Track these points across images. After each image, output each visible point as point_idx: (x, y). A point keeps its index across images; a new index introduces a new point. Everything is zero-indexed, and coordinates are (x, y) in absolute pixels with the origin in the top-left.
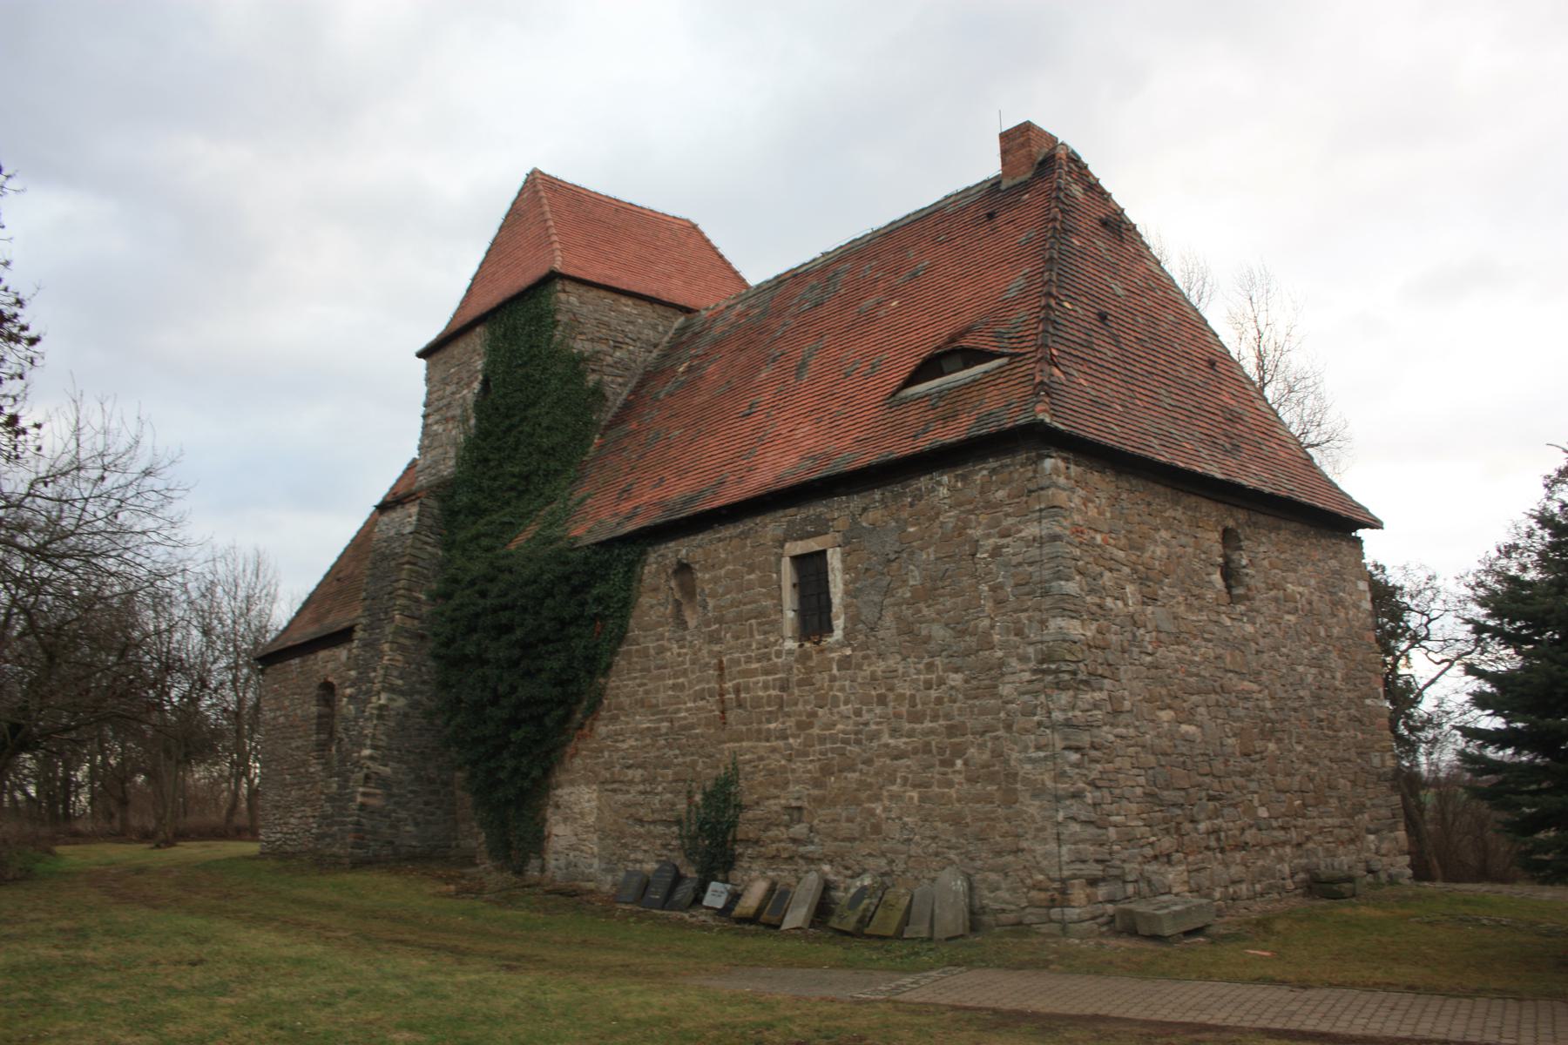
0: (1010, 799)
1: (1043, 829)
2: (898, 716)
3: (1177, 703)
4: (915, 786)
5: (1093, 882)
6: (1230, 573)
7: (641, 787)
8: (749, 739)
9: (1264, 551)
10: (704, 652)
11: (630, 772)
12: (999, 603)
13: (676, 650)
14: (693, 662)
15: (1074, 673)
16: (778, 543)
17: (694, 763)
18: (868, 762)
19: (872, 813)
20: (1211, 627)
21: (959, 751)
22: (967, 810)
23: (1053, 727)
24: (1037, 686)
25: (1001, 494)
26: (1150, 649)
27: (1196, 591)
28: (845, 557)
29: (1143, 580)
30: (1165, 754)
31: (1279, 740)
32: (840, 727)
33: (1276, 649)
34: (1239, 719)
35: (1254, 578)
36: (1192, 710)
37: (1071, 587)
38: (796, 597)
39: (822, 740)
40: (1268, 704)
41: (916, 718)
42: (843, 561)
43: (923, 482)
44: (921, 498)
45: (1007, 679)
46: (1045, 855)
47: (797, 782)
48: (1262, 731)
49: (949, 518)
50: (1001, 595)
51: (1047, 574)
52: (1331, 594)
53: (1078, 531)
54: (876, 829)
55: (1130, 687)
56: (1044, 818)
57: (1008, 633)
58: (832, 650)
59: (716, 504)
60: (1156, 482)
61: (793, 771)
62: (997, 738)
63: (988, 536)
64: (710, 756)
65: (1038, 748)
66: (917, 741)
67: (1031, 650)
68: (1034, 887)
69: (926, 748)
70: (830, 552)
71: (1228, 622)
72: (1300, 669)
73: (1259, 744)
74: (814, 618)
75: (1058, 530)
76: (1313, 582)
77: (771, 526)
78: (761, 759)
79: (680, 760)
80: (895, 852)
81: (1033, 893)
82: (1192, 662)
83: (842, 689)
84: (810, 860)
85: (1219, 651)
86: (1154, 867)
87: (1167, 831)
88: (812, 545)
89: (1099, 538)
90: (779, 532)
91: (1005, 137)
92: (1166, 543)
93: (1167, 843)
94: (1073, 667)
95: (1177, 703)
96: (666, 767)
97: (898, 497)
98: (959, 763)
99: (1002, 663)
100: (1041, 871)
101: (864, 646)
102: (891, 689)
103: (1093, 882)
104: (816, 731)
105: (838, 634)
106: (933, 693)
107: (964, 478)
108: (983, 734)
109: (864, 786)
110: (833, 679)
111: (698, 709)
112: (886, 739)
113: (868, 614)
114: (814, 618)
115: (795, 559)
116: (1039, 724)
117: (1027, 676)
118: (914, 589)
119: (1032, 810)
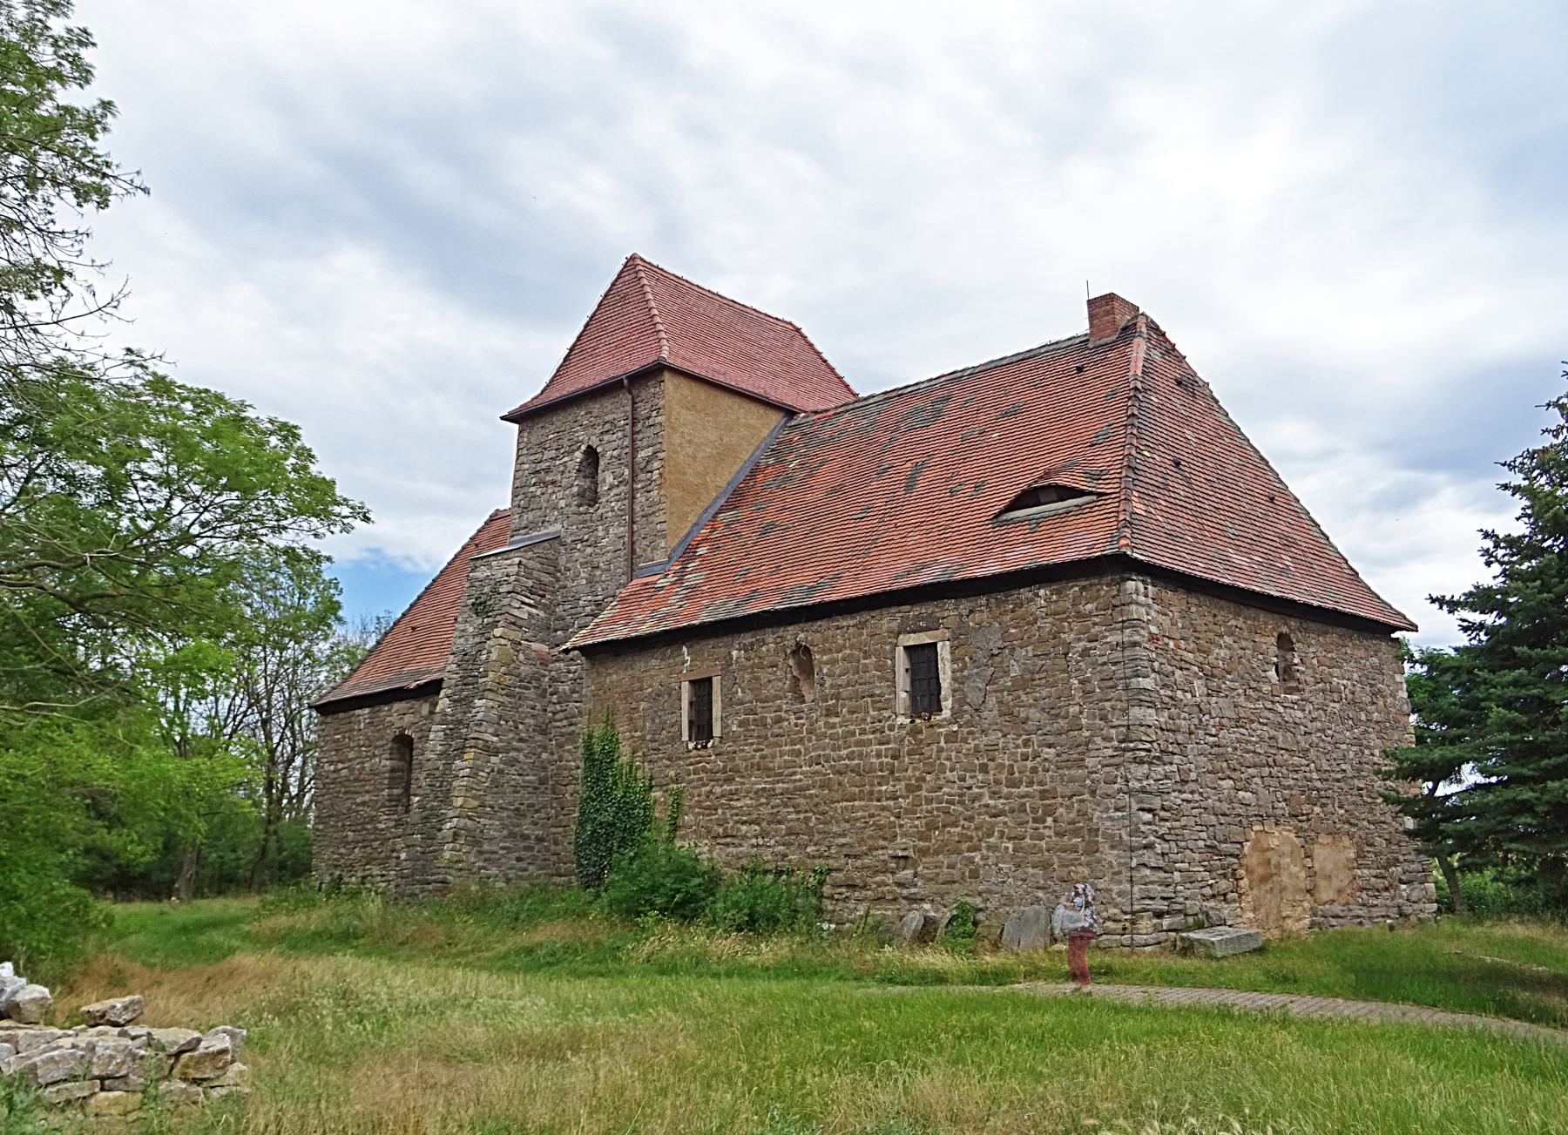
0: (1092, 849)
1: (1120, 873)
2: (998, 782)
3: (1235, 775)
4: (1010, 839)
5: (1159, 915)
6: (1286, 672)
7: (754, 841)
8: (862, 799)
9: (1312, 650)
10: (821, 723)
11: (744, 828)
12: (1087, 693)
13: (793, 721)
14: (810, 732)
15: (1149, 751)
16: (895, 637)
17: (807, 819)
18: (970, 819)
19: (971, 861)
20: (1266, 714)
21: (1050, 811)
22: (1055, 859)
23: (1130, 793)
24: (1116, 760)
25: (1089, 606)
26: (1214, 731)
27: (1254, 685)
28: (953, 649)
29: (1209, 677)
30: (1224, 815)
31: (1323, 805)
32: (945, 790)
33: (1323, 731)
34: (1289, 787)
35: (1304, 674)
36: (1249, 780)
37: (1147, 683)
38: (908, 680)
39: (929, 801)
40: (1315, 776)
41: (1014, 784)
42: (952, 653)
43: (1025, 593)
44: (1021, 606)
45: (1093, 753)
46: (1120, 894)
47: (904, 835)
48: (1309, 798)
49: (1047, 625)
50: (1088, 687)
51: (1129, 672)
52: (1372, 686)
53: (1153, 638)
54: (974, 874)
55: (1195, 761)
56: (1120, 864)
57: (1094, 717)
58: (940, 726)
59: (834, 597)
60: (1221, 598)
61: (901, 826)
62: (1083, 801)
63: (1079, 640)
64: (824, 813)
65: (1117, 810)
66: (1015, 803)
67: (1113, 731)
68: (1109, 919)
69: (1022, 808)
70: (939, 645)
71: (1281, 710)
72: (1344, 747)
73: (1306, 808)
74: (926, 695)
75: (1137, 638)
76: (1355, 676)
77: (887, 621)
78: (872, 816)
79: (794, 816)
80: (990, 892)
81: (1109, 924)
82: (1248, 742)
83: (948, 759)
84: (913, 899)
85: (1273, 732)
86: (1212, 904)
87: (1225, 876)
88: (924, 638)
89: (1172, 644)
90: (894, 625)
91: (1091, 303)
92: (1229, 647)
93: (1224, 885)
94: (1148, 746)
95: (1235, 775)
96: (780, 822)
97: (999, 603)
98: (1050, 820)
99: (1089, 741)
100: (1116, 906)
101: (969, 724)
102: (993, 760)
103: (1159, 915)
104: (924, 793)
105: (946, 713)
106: (1029, 764)
107: (1058, 592)
108: (1070, 798)
109: (965, 838)
110: (940, 750)
111: (816, 773)
112: (986, 800)
113: (974, 697)
114: (926, 695)
115: (906, 648)
116: (1120, 791)
117: (1110, 752)
118: (1014, 680)
119: (1109, 858)
